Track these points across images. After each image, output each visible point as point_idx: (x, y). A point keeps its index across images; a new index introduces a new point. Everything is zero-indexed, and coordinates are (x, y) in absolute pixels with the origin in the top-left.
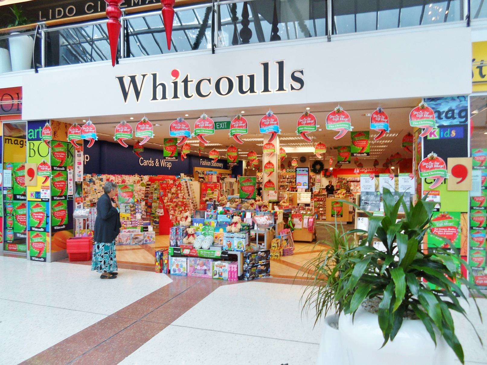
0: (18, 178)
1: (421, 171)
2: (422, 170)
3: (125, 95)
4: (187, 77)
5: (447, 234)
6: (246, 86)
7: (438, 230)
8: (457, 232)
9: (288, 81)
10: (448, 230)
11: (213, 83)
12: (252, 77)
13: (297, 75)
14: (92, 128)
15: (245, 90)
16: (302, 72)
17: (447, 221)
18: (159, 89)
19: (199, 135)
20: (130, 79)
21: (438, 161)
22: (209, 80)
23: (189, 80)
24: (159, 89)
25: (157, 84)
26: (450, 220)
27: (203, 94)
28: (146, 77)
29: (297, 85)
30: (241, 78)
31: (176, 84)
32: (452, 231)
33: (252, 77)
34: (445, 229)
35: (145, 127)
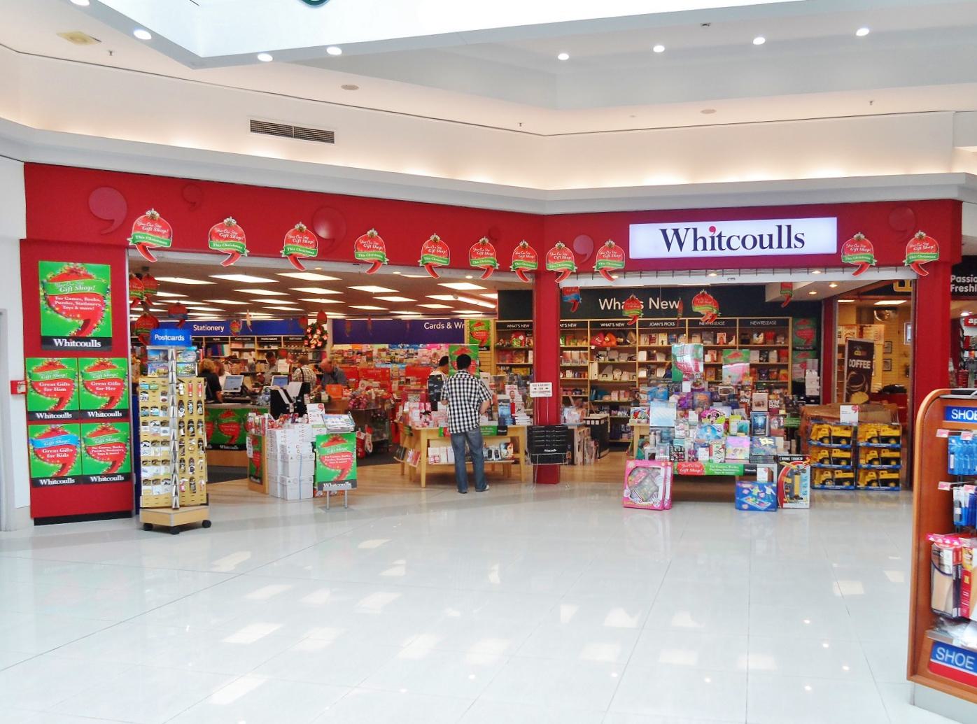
0: (56, 298)
1: (211, 239)
2: (213, 238)
3: (669, 245)
4: (721, 233)
5: (81, 308)
6: (766, 243)
7: (64, 301)
8: (104, 305)
9: (793, 241)
10: (84, 301)
11: (741, 238)
12: (771, 236)
13: (799, 236)
14: (377, 244)
15: (764, 246)
16: (803, 234)
17: (83, 283)
18: (700, 243)
19: (602, 269)
20: (673, 232)
21: (236, 230)
22: (738, 237)
23: (723, 235)
24: (700, 243)
25: (698, 237)
26: (89, 280)
27: (752, 238)
28: (689, 230)
29: (799, 244)
30: (761, 236)
31: (713, 238)
32: (93, 302)
33: (771, 236)
34: (77, 299)
35: (484, 252)
